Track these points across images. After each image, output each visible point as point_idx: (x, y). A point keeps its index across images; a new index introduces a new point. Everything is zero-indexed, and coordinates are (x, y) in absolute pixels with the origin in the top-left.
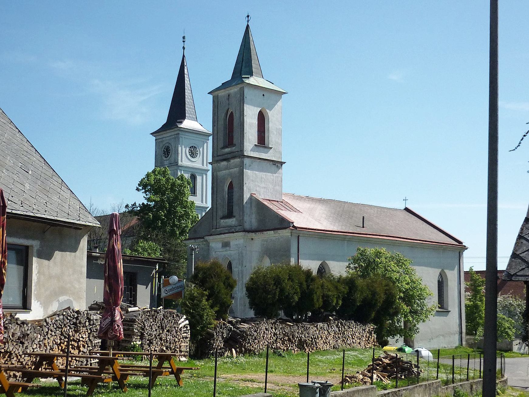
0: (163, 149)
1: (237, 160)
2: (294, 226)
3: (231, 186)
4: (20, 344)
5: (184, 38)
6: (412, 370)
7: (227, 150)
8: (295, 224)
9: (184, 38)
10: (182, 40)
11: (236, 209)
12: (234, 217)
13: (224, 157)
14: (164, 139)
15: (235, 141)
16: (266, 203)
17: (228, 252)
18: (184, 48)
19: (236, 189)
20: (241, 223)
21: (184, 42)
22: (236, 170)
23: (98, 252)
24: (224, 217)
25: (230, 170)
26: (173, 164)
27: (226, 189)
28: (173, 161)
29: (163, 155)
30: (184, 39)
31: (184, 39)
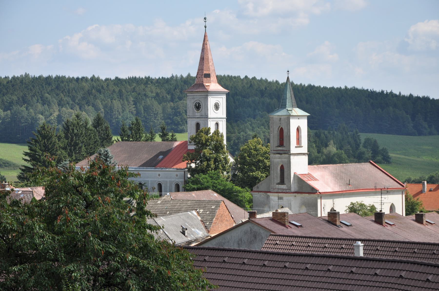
0: (194, 104)
1: (287, 155)
2: (319, 192)
3: (282, 168)
4: (67, 263)
5: (205, 19)
6: (140, 287)
7: (280, 148)
8: (320, 191)
9: (205, 19)
10: (203, 20)
11: (286, 180)
12: (285, 184)
13: (278, 152)
14: (195, 97)
15: (285, 144)
16: (300, 176)
17: (282, 202)
18: (205, 27)
19: (285, 170)
20: (290, 189)
21: (205, 22)
22: (286, 160)
23: (362, 254)
24: (278, 184)
25: (282, 159)
26: (204, 116)
27: (279, 168)
28: (203, 114)
29: (194, 108)
30: (205, 19)
31: (205, 19)
